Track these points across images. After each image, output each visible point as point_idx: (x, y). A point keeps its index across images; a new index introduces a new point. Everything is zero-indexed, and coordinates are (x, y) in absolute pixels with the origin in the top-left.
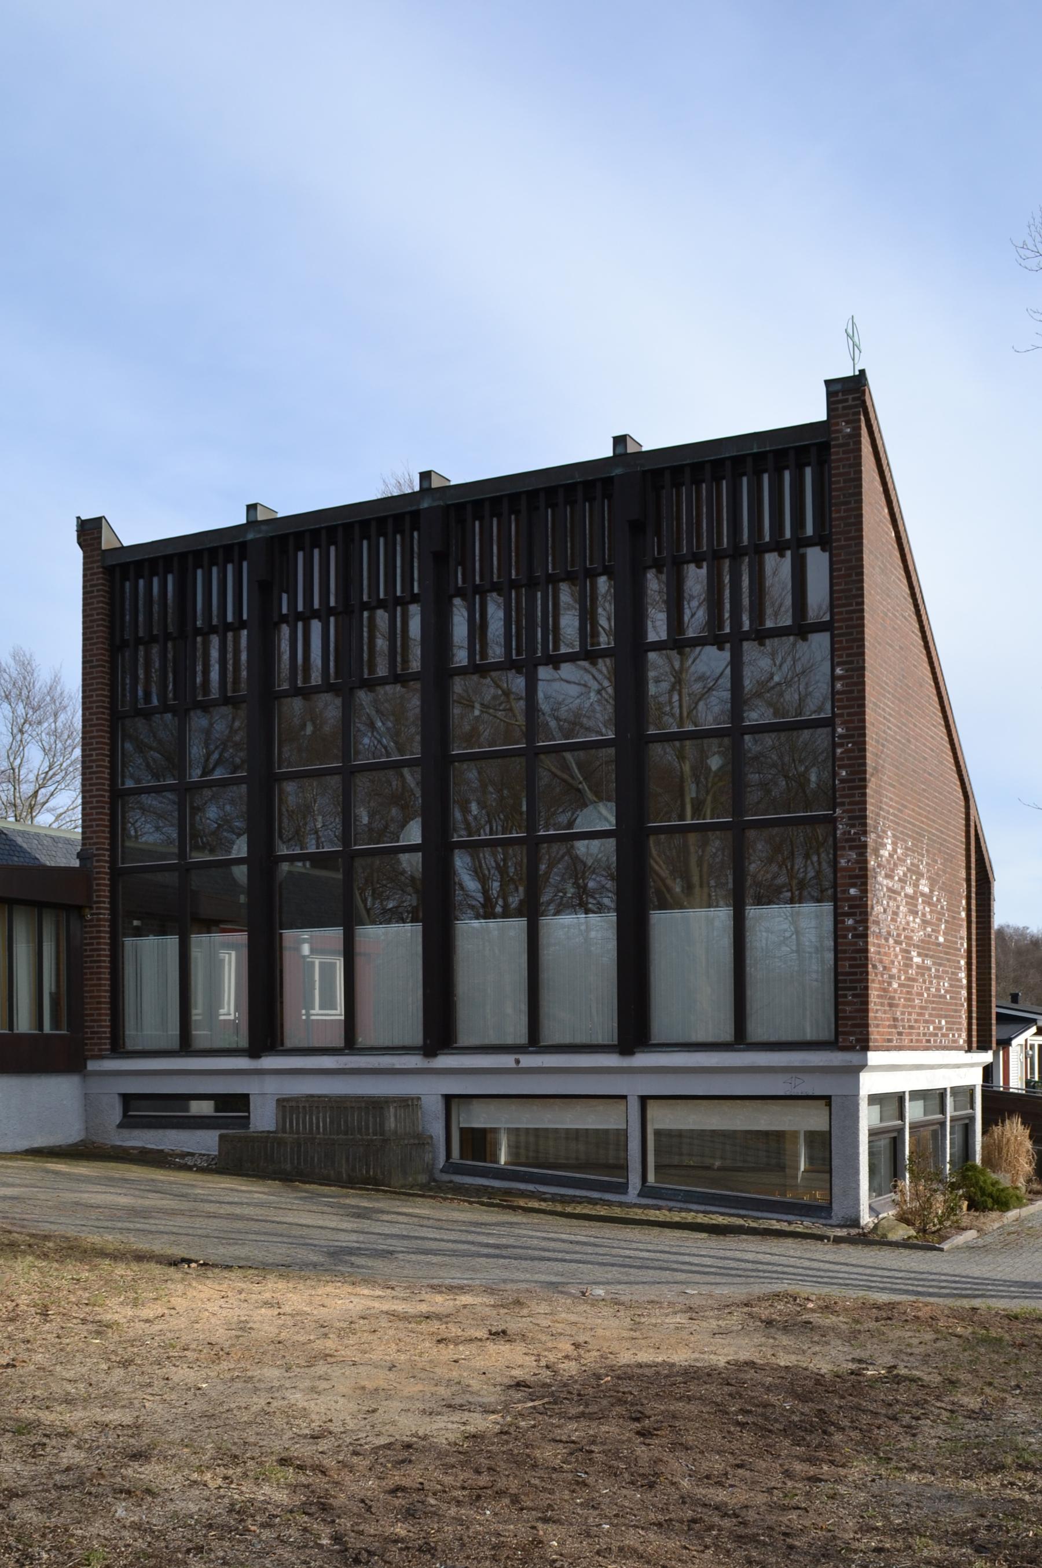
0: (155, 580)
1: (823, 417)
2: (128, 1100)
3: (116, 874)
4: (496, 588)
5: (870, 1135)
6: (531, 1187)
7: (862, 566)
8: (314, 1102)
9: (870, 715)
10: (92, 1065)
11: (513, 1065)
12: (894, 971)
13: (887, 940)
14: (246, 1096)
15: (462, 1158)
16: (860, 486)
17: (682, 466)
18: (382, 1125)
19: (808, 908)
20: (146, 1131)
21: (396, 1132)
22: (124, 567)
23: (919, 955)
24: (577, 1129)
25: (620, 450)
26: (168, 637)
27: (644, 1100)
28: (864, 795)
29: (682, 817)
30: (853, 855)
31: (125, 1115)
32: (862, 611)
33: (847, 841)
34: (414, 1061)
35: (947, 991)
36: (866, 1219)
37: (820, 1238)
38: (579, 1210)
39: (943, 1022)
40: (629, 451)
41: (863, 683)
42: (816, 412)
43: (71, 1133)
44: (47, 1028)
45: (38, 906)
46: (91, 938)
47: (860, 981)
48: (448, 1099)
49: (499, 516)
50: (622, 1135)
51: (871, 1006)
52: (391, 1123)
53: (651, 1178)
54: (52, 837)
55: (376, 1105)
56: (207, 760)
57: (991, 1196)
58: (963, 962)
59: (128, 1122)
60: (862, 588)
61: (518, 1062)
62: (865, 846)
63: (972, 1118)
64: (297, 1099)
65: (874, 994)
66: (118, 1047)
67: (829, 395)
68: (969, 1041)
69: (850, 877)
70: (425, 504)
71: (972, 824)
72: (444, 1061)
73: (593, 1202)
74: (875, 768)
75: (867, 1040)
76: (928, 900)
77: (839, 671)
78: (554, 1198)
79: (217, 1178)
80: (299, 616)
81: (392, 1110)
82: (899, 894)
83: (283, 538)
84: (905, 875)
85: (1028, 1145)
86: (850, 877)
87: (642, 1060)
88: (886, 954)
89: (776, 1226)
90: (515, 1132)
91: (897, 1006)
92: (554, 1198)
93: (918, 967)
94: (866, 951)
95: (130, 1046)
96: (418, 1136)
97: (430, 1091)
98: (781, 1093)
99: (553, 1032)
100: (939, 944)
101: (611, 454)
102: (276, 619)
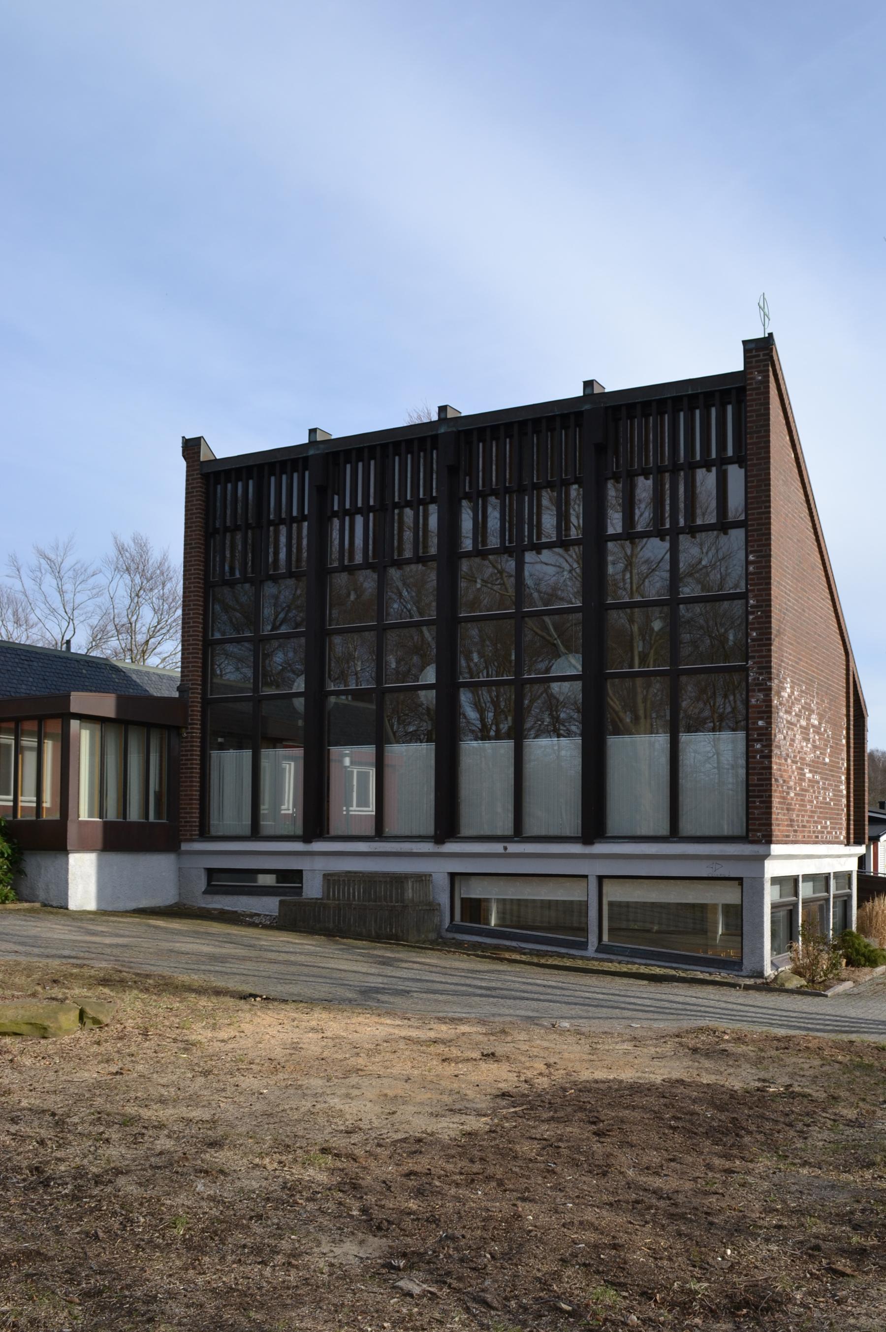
1: (741, 368)
2: (211, 873)
5: (772, 908)
7: (769, 479)
8: (351, 877)
9: (775, 591)
10: (185, 847)
11: (503, 851)
12: (792, 783)
13: (786, 760)
14: (300, 872)
15: (462, 921)
16: (769, 419)
20: (224, 897)
22: (217, 474)
23: (810, 771)
24: (550, 901)
25: (588, 391)
26: (248, 526)
27: (601, 879)
28: (770, 650)
29: (631, 666)
31: (209, 884)
32: (769, 512)
33: (756, 685)
34: (427, 847)
35: (831, 800)
36: (769, 971)
37: (733, 986)
39: (828, 823)
42: (736, 364)
43: (167, 896)
44: (152, 818)
45: (147, 726)
46: (186, 751)
47: (766, 791)
48: (453, 876)
51: (774, 810)
52: (409, 894)
53: (605, 938)
55: (398, 880)
57: (863, 955)
58: (843, 778)
59: (211, 890)
60: (769, 496)
61: (505, 848)
63: (850, 896)
66: (204, 834)
67: (746, 351)
68: (848, 837)
69: (759, 712)
71: (851, 673)
72: (451, 847)
74: (778, 631)
75: (771, 836)
76: (817, 731)
77: (751, 558)
78: (531, 953)
81: (410, 884)
83: (336, 454)
84: (800, 711)
86: (759, 712)
87: (599, 848)
88: (785, 771)
89: (701, 976)
91: (793, 810)
93: (810, 781)
94: (770, 768)
95: (214, 832)
96: (430, 904)
97: (439, 870)
100: (825, 764)
101: (581, 394)
102: (329, 514)
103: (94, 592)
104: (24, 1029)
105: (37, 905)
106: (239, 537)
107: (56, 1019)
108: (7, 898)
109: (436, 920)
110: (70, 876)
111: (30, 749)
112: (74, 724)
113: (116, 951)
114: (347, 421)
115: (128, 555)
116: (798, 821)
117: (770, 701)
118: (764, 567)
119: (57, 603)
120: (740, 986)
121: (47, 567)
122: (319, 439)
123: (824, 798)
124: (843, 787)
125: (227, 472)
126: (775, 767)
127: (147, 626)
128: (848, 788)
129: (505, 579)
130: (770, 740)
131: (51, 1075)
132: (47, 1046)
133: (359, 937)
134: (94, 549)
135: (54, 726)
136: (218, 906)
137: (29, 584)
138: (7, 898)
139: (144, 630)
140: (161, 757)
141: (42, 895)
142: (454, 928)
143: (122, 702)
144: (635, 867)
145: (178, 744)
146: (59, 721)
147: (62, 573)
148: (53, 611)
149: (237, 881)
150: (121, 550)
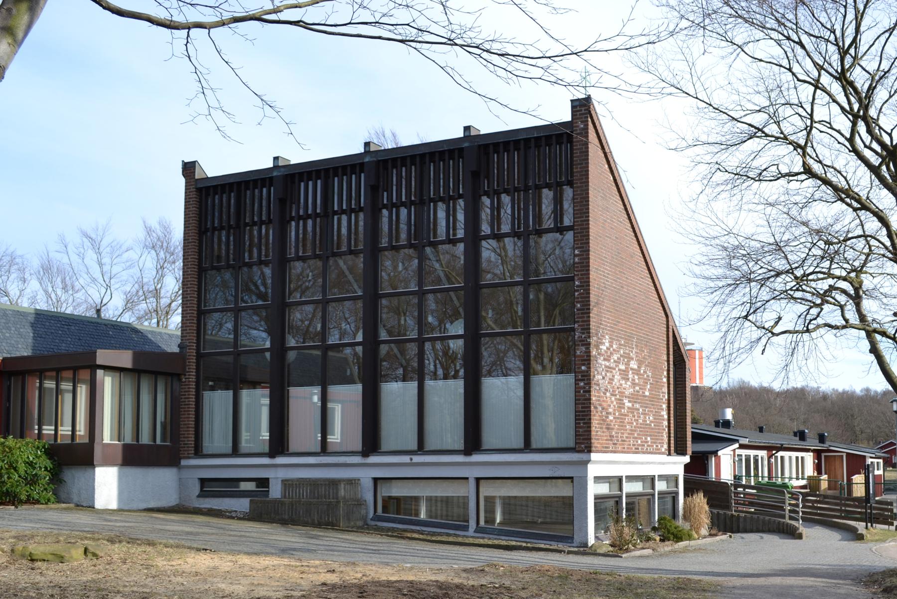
0: (265, 190)
1: (570, 119)
2: (203, 481)
3: (199, 356)
4: (442, 199)
5: (595, 499)
8: (302, 482)
10: (184, 462)
11: (409, 461)
12: (611, 410)
13: (605, 394)
14: (268, 479)
16: (588, 155)
17: (499, 143)
18: (337, 493)
22: (208, 188)
23: (629, 401)
24: (447, 497)
25: (467, 134)
26: (230, 227)
27: (478, 480)
28: (589, 317)
29: (539, 325)
30: (583, 349)
31: (201, 490)
32: (588, 220)
34: (357, 459)
35: (651, 422)
36: (591, 541)
37: (560, 551)
38: (439, 538)
40: (472, 134)
42: (566, 116)
43: (171, 500)
44: (158, 442)
45: (155, 374)
47: (587, 415)
48: (376, 480)
49: (508, 151)
50: (466, 498)
51: (593, 429)
52: (342, 493)
53: (482, 523)
55: (334, 483)
56: (822, 279)
57: (673, 534)
59: (203, 494)
61: (411, 459)
62: (589, 344)
63: (677, 493)
66: (198, 452)
67: (573, 107)
69: (582, 360)
70: (367, 160)
71: (671, 330)
72: (373, 459)
73: (448, 535)
74: (597, 303)
75: (590, 447)
76: (636, 372)
77: (576, 252)
78: (429, 534)
79: (246, 522)
80: (394, 205)
81: (342, 486)
83: (292, 176)
85: (707, 507)
86: (582, 360)
87: (476, 458)
89: (542, 546)
91: (613, 429)
92: (429, 534)
93: (629, 408)
94: (590, 399)
95: (205, 451)
96: (358, 500)
97: (366, 476)
98: (548, 476)
101: (462, 135)
103: (128, 264)
104: (50, 557)
105: (72, 505)
106: (224, 233)
107: (69, 552)
108: (49, 500)
109: (363, 512)
110: (96, 484)
111: (68, 391)
112: (100, 373)
113: (121, 529)
114: (296, 156)
119: (97, 274)
121: (89, 244)
122: (280, 164)
123: (645, 421)
124: (664, 413)
126: (593, 398)
128: (669, 414)
129: (441, 257)
130: (590, 379)
131: (64, 578)
132: (63, 566)
133: (305, 524)
134: (127, 231)
135: (85, 374)
136: (209, 506)
137: (75, 258)
138: (49, 500)
141: (75, 499)
142: (377, 518)
143: (137, 356)
144: (503, 471)
145: (179, 384)
146: (89, 371)
147: (101, 249)
148: (94, 280)
149: (225, 487)
150: (149, 231)
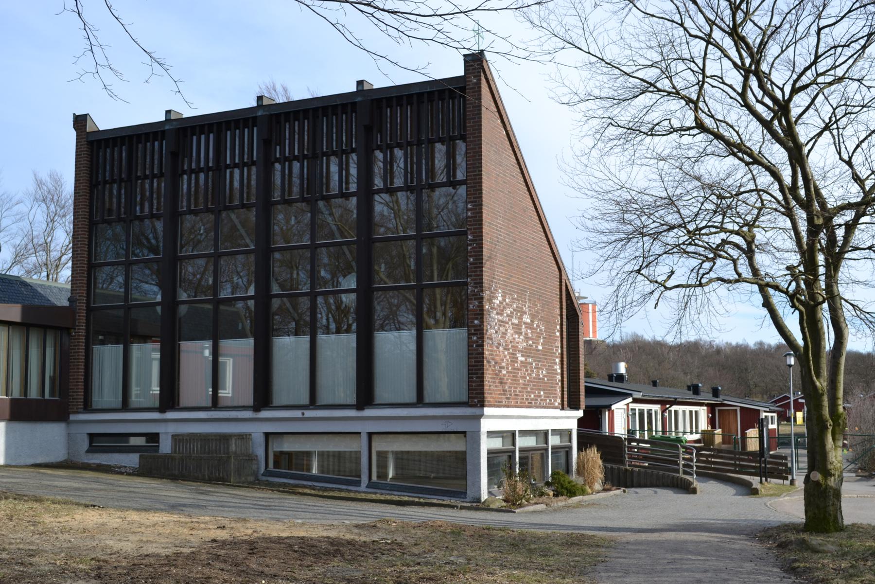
1: (462, 74)
2: (92, 437)
3: (89, 310)
4: (334, 153)
5: (488, 453)
6: (310, 483)
7: (481, 152)
8: (193, 437)
9: (486, 229)
10: (72, 417)
12: (504, 364)
13: (498, 348)
14: (158, 434)
15: (275, 467)
18: (228, 448)
19: (149, 346)
21: (235, 453)
22: (99, 141)
23: (522, 356)
25: (360, 88)
26: (121, 180)
27: (370, 435)
28: (482, 271)
29: (432, 279)
31: (90, 445)
33: (473, 295)
35: (544, 376)
36: (484, 496)
37: (453, 507)
38: (331, 494)
39: (542, 393)
40: (365, 88)
41: (481, 212)
42: (458, 70)
43: (60, 455)
44: (47, 396)
45: (45, 328)
48: (267, 435)
50: (358, 454)
51: (486, 383)
52: (233, 448)
53: (374, 478)
54: (59, 289)
55: (225, 438)
57: (566, 488)
58: (558, 360)
59: (92, 449)
60: (481, 163)
61: (303, 414)
62: (482, 298)
64: (182, 435)
65: (488, 377)
66: (88, 407)
67: (466, 62)
68: (563, 404)
70: (259, 113)
71: (564, 284)
72: (265, 414)
73: (340, 490)
74: (489, 257)
75: (483, 401)
76: (529, 326)
78: (321, 489)
80: (286, 159)
81: (233, 441)
82: (507, 323)
84: (511, 313)
87: (368, 412)
88: (497, 355)
89: (435, 501)
90: (321, 454)
91: (506, 383)
92: (321, 489)
93: (522, 362)
94: (483, 353)
95: (94, 407)
97: (257, 431)
99: (324, 397)
100: (539, 350)
101: (355, 90)
102: (180, 172)
103: (18, 217)
109: (254, 467)
115: (45, 188)
116: (510, 391)
117: (483, 306)
118: (478, 213)
120: (457, 507)
124: (558, 368)
125: (107, 140)
127: (61, 245)
128: (562, 368)
133: (195, 480)
136: (97, 462)
139: (58, 248)
140: (55, 350)
142: (268, 473)
143: (26, 311)
144: (397, 426)
149: (115, 442)
150: (40, 184)
